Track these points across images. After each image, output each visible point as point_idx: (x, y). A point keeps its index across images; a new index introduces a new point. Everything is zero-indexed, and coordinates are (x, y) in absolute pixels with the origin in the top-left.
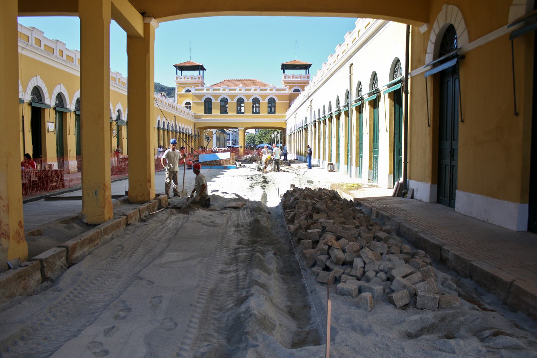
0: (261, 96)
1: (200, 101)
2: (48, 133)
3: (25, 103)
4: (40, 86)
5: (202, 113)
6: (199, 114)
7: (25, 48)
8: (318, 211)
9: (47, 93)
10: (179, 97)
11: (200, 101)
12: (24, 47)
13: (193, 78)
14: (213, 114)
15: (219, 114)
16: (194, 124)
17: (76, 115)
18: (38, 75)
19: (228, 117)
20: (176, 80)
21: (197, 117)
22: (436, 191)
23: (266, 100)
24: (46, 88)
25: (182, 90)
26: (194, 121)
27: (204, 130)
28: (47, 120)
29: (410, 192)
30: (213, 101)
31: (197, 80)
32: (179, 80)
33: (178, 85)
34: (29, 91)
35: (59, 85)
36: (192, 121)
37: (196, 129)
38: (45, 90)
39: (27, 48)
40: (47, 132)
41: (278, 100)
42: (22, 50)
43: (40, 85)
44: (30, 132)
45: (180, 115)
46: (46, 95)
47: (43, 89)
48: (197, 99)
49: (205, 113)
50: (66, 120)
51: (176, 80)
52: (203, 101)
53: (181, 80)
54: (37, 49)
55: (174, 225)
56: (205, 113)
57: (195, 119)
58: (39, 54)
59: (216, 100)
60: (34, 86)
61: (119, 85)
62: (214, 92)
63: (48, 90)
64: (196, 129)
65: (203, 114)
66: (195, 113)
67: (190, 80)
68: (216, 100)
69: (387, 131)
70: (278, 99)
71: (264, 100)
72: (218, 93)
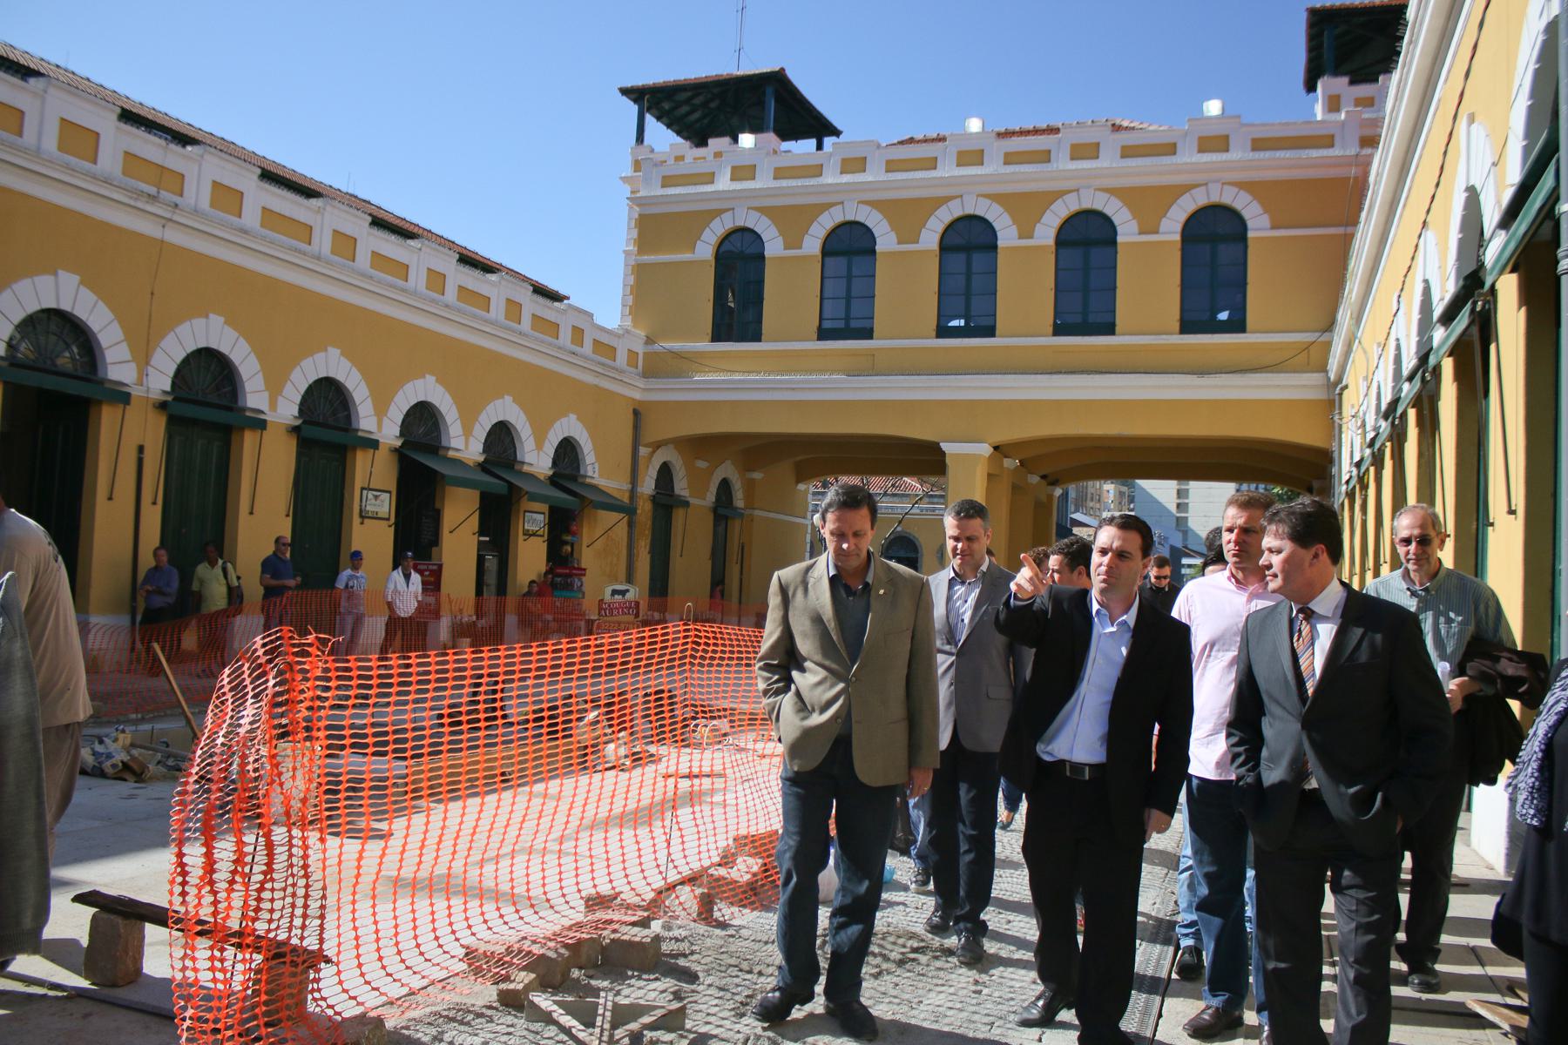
0: (1126, 195)
2: (362, 523)
3: (133, 401)
4: (513, 422)
6: (676, 345)
7: (170, 220)
9: (532, 438)
12: (168, 215)
16: (636, 413)
17: (177, 423)
19: (871, 367)
23: (1172, 227)
24: (454, 408)
27: (802, 474)
28: (358, 484)
30: (774, 247)
34: (481, 433)
39: (176, 218)
40: (356, 519)
41: (1265, 221)
42: (164, 227)
44: (288, 515)
47: (582, 444)
49: (717, 337)
50: (354, 474)
52: (705, 250)
54: (433, 301)
55: (790, 838)
58: (374, 292)
59: (793, 242)
60: (494, 421)
63: (370, 390)
68: (793, 242)
69: (1512, 512)
70: (1266, 209)
71: (1149, 228)
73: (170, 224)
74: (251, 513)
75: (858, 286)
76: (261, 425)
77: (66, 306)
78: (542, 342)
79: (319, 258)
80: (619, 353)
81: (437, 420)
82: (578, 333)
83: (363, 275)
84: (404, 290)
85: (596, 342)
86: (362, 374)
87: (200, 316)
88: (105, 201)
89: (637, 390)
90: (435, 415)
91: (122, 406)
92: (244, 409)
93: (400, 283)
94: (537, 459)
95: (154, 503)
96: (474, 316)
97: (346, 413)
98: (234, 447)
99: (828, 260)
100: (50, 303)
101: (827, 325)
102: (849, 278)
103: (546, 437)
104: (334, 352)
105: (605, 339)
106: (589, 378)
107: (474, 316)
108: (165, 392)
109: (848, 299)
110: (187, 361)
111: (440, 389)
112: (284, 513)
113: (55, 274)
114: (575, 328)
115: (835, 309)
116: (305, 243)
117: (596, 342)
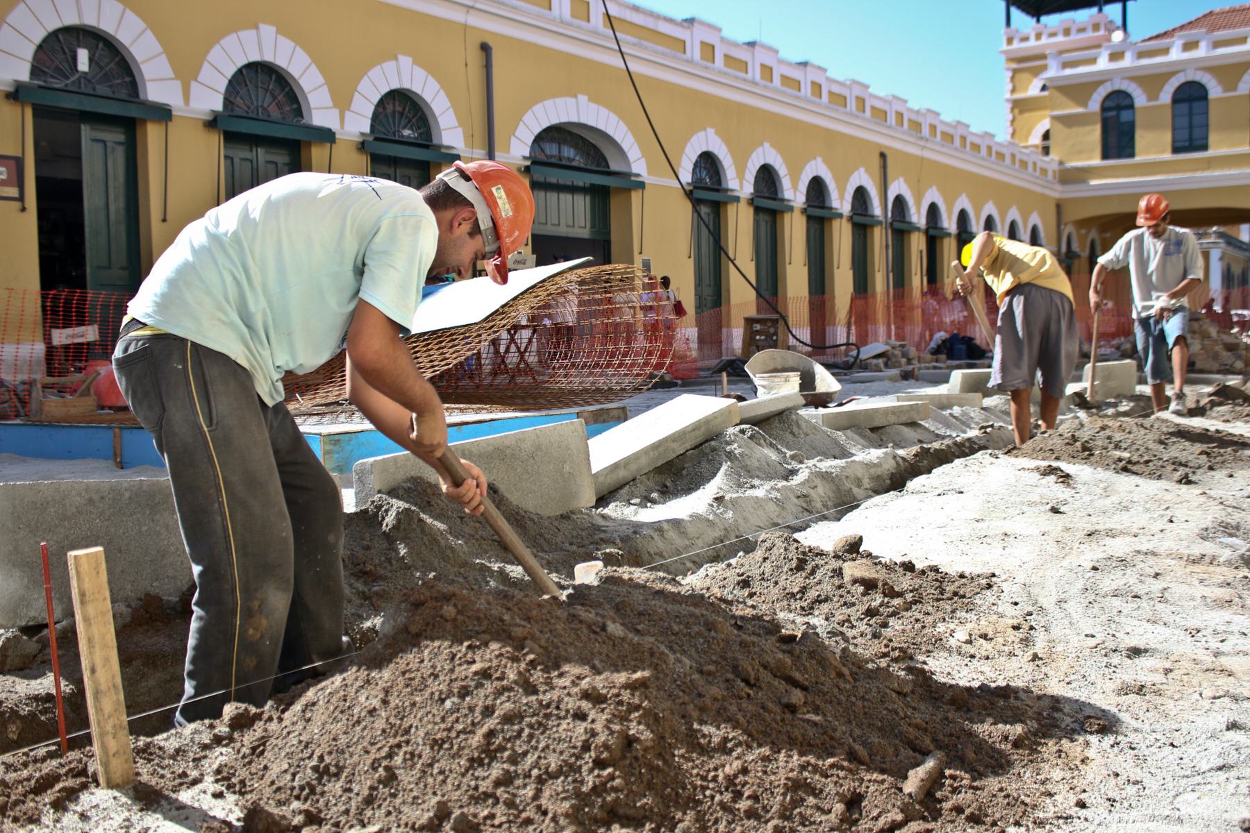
1: (1080, 110)
5: (1090, 158)
7: (472, 7)
8: (1030, 614)
9: (733, 167)
10: (1016, 111)
11: (1080, 110)
13: (1073, 31)
14: (1138, 158)
15: (1168, 156)
17: (810, 218)
18: (265, 22)
20: (1005, 47)
21: (1069, 177)
22: (591, 458)
25: (1030, 82)
26: (1057, 195)
29: (73, 336)
31: (1090, 34)
32: (1016, 45)
33: (1014, 66)
34: (751, 175)
35: (393, 63)
36: (1045, 197)
37: (1068, 229)
38: (782, 170)
42: (468, 12)
43: (770, 161)
45: (927, 154)
46: (913, 209)
48: (1070, 103)
49: (1105, 156)
51: (1005, 47)
52: (1095, 105)
53: (1024, 45)
56: (1105, 156)
57: (1059, 187)
59: (1153, 96)
60: (699, 152)
61: (765, 87)
62: (1145, 62)
64: (1068, 229)
65: (1096, 161)
66: (1061, 163)
67: (1060, 38)
68: (1153, 96)
72: (1161, 64)
73: (471, 11)
74: (164, 220)
75: (1197, 120)
76: (737, 199)
77: (268, 57)
78: (657, 52)
79: (562, 22)
80: (923, 127)
81: (423, 114)
82: (963, 139)
83: (720, 72)
84: (797, 98)
85: (727, 57)
86: (628, 126)
87: (700, 130)
88: (600, 49)
89: (1057, 192)
90: (288, 84)
91: (329, 145)
92: (440, 147)
93: (743, 75)
94: (918, 217)
95: (527, 245)
96: (737, 78)
97: (295, 106)
98: (906, 242)
99: (1177, 106)
100: (255, 57)
101: (1179, 144)
102: (1191, 115)
103: (521, 120)
104: (405, 61)
105: (879, 105)
106: (1039, 190)
107: (737, 78)
108: (525, 158)
109: (1191, 127)
110: (382, 103)
111: (420, 73)
112: (687, 255)
113: (257, 27)
114: (814, 83)
115: (1184, 135)
116: (545, 8)
117: (727, 57)
